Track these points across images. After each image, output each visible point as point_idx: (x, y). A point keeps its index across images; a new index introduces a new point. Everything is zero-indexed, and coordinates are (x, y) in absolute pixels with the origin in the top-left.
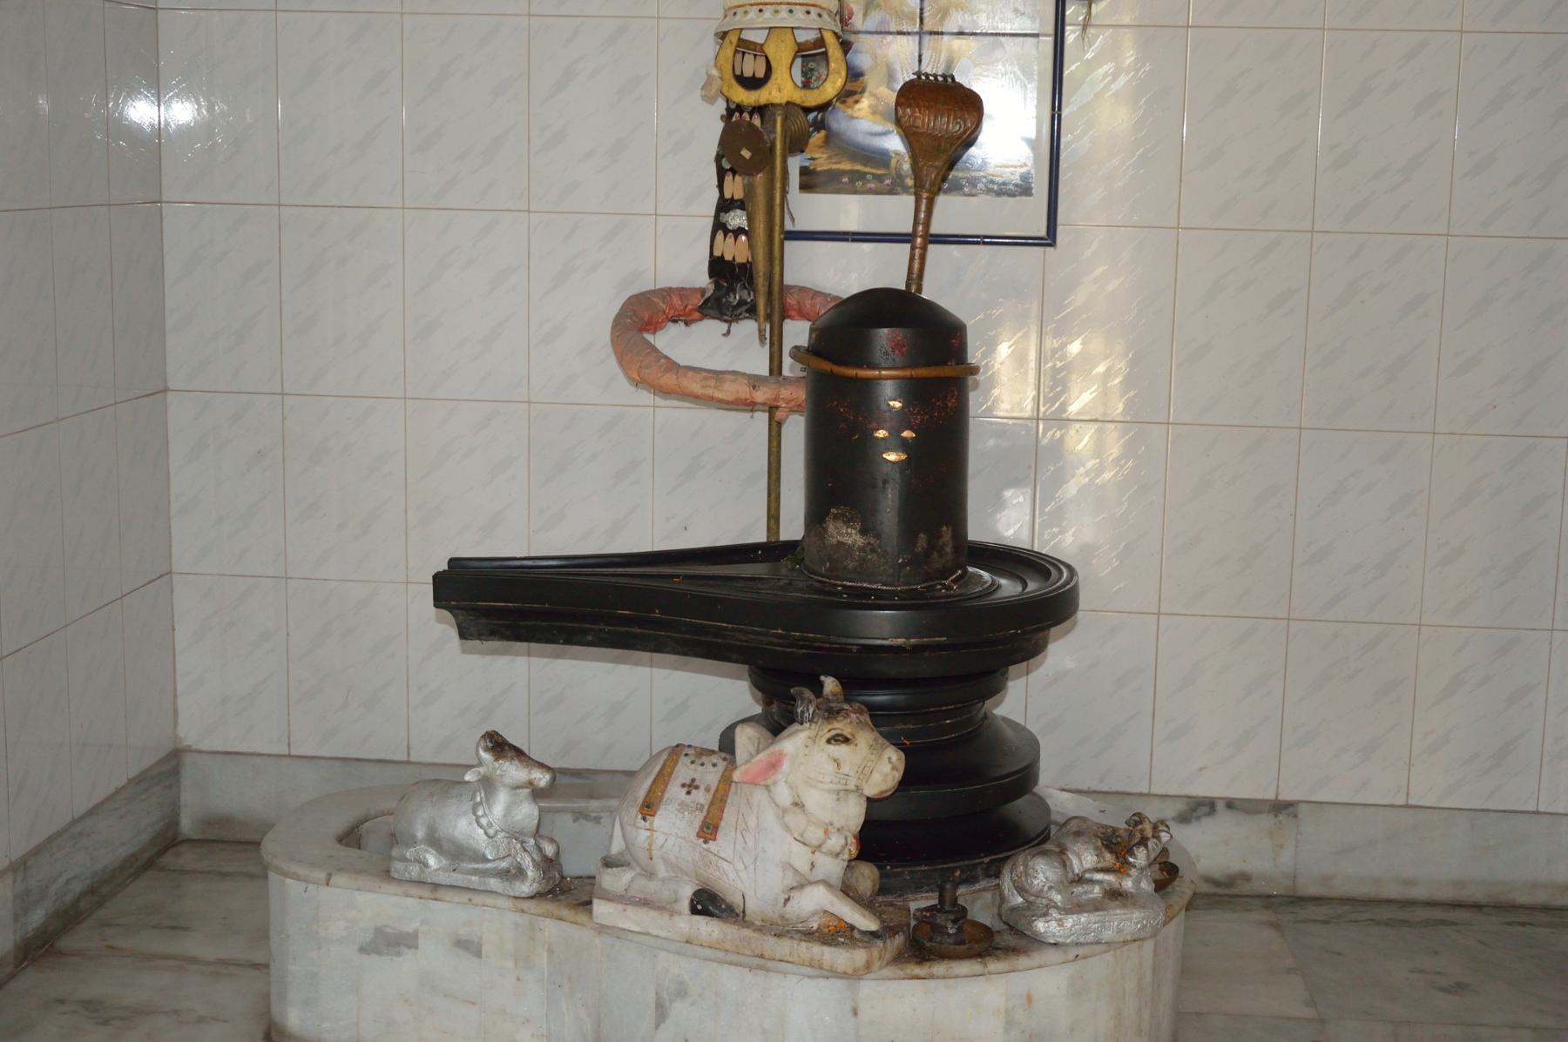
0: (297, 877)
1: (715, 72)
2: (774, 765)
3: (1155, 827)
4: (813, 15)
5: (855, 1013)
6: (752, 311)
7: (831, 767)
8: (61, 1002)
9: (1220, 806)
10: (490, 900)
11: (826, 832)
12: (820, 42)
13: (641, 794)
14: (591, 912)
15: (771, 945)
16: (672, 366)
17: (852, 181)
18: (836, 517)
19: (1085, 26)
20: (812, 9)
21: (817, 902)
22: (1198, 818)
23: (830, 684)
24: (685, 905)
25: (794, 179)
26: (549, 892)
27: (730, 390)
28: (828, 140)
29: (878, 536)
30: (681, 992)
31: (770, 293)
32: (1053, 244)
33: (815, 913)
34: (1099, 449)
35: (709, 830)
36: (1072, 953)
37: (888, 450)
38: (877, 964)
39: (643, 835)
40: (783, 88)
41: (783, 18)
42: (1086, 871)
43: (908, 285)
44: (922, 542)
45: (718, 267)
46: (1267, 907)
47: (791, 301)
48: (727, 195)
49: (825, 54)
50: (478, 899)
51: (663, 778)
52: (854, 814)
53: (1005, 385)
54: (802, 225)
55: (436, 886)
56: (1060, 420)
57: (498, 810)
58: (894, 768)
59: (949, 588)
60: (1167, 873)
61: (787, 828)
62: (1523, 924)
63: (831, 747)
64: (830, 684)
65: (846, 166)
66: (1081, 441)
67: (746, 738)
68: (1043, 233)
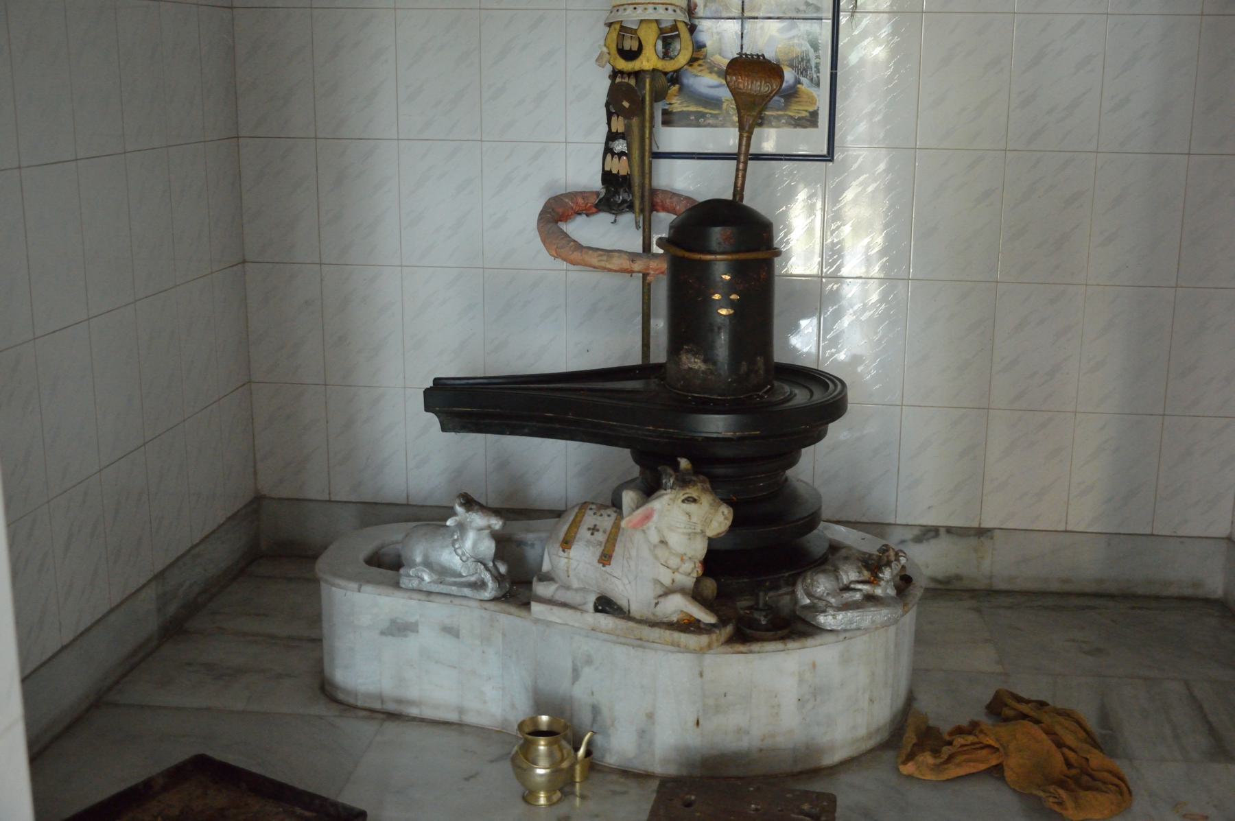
0: (340, 587)
1: (605, 50)
2: (648, 517)
3: (897, 554)
4: (670, 11)
5: (701, 675)
6: (631, 207)
7: (685, 518)
8: (189, 664)
9: (942, 531)
10: (465, 602)
11: (682, 560)
12: (675, 28)
13: (562, 535)
14: (529, 609)
15: (647, 631)
16: (579, 247)
17: (697, 120)
18: (687, 351)
19: (853, 12)
20: (670, 7)
21: (678, 606)
22: (928, 539)
23: (684, 463)
24: (591, 606)
25: (659, 117)
26: (504, 596)
27: (617, 263)
28: (680, 90)
29: (715, 363)
30: (589, 661)
31: (642, 197)
32: (832, 160)
33: (675, 612)
34: (865, 293)
35: (605, 558)
36: (842, 636)
37: (722, 307)
38: (715, 644)
39: (564, 561)
40: (649, 61)
41: (651, 14)
42: (852, 582)
43: (734, 195)
44: (744, 367)
45: (607, 177)
46: (972, 598)
47: (658, 199)
48: (614, 130)
49: (678, 36)
50: (457, 601)
51: (576, 524)
52: (699, 549)
53: (799, 255)
54: (664, 148)
55: (429, 593)
56: (837, 278)
57: (468, 544)
58: (726, 518)
59: (762, 397)
60: (904, 582)
61: (656, 558)
62: (1140, 608)
63: (685, 506)
64: (684, 463)
65: (693, 108)
66: (851, 291)
67: (628, 497)
68: (825, 152)
